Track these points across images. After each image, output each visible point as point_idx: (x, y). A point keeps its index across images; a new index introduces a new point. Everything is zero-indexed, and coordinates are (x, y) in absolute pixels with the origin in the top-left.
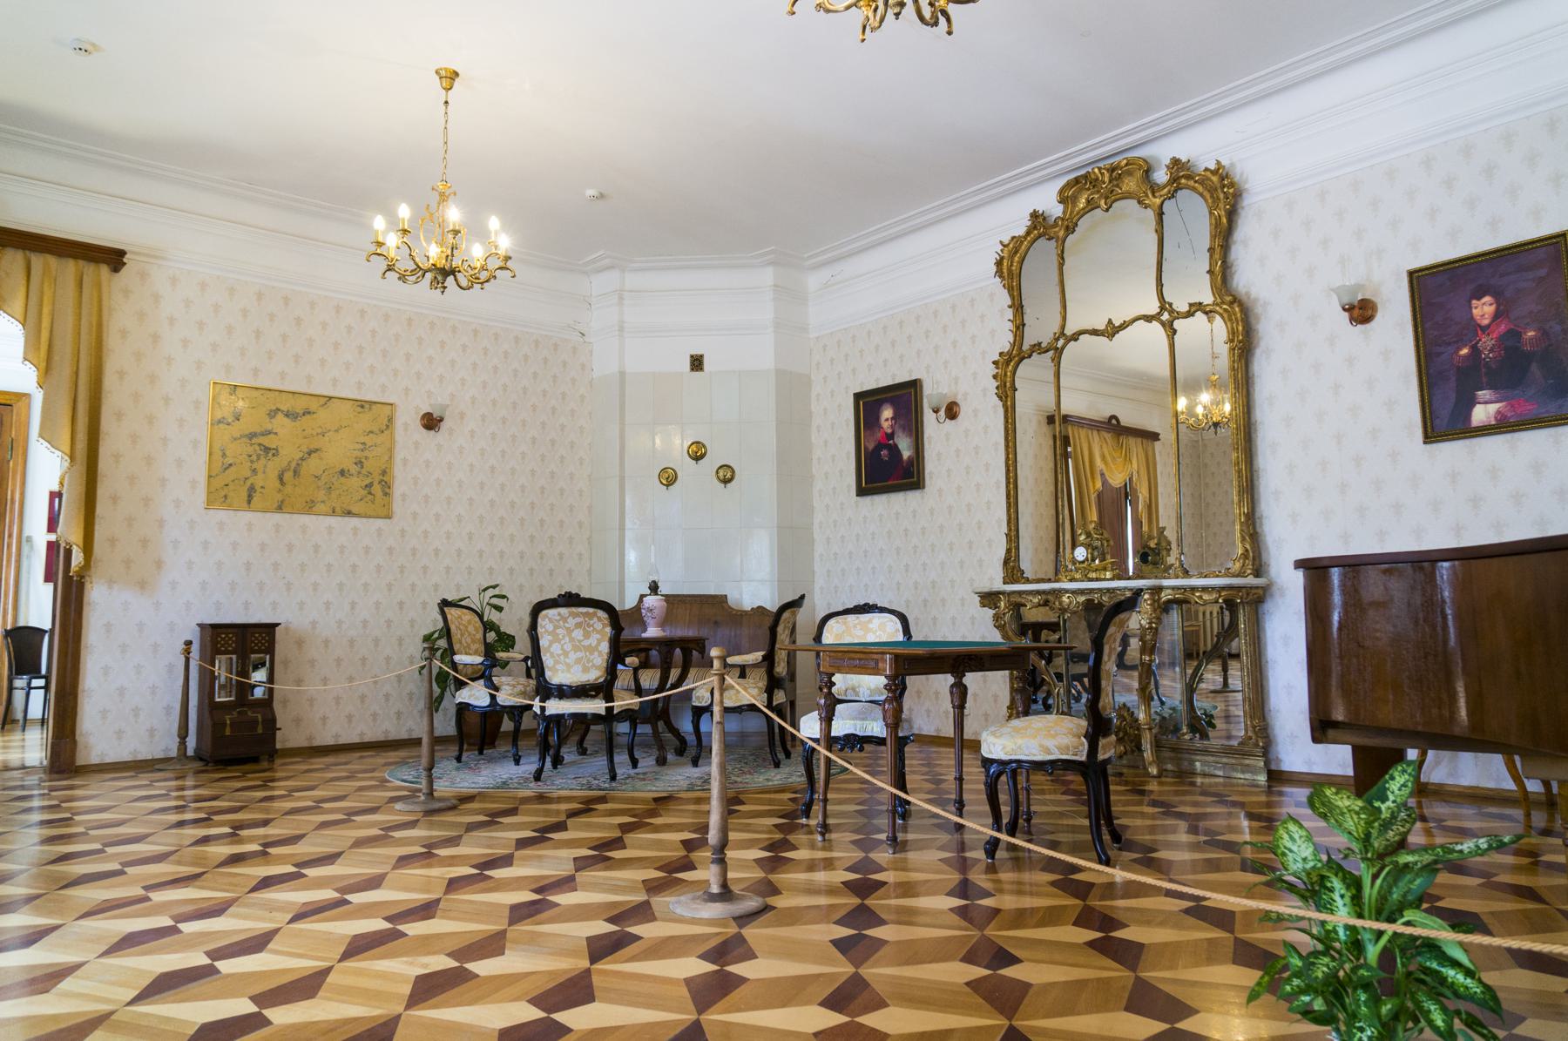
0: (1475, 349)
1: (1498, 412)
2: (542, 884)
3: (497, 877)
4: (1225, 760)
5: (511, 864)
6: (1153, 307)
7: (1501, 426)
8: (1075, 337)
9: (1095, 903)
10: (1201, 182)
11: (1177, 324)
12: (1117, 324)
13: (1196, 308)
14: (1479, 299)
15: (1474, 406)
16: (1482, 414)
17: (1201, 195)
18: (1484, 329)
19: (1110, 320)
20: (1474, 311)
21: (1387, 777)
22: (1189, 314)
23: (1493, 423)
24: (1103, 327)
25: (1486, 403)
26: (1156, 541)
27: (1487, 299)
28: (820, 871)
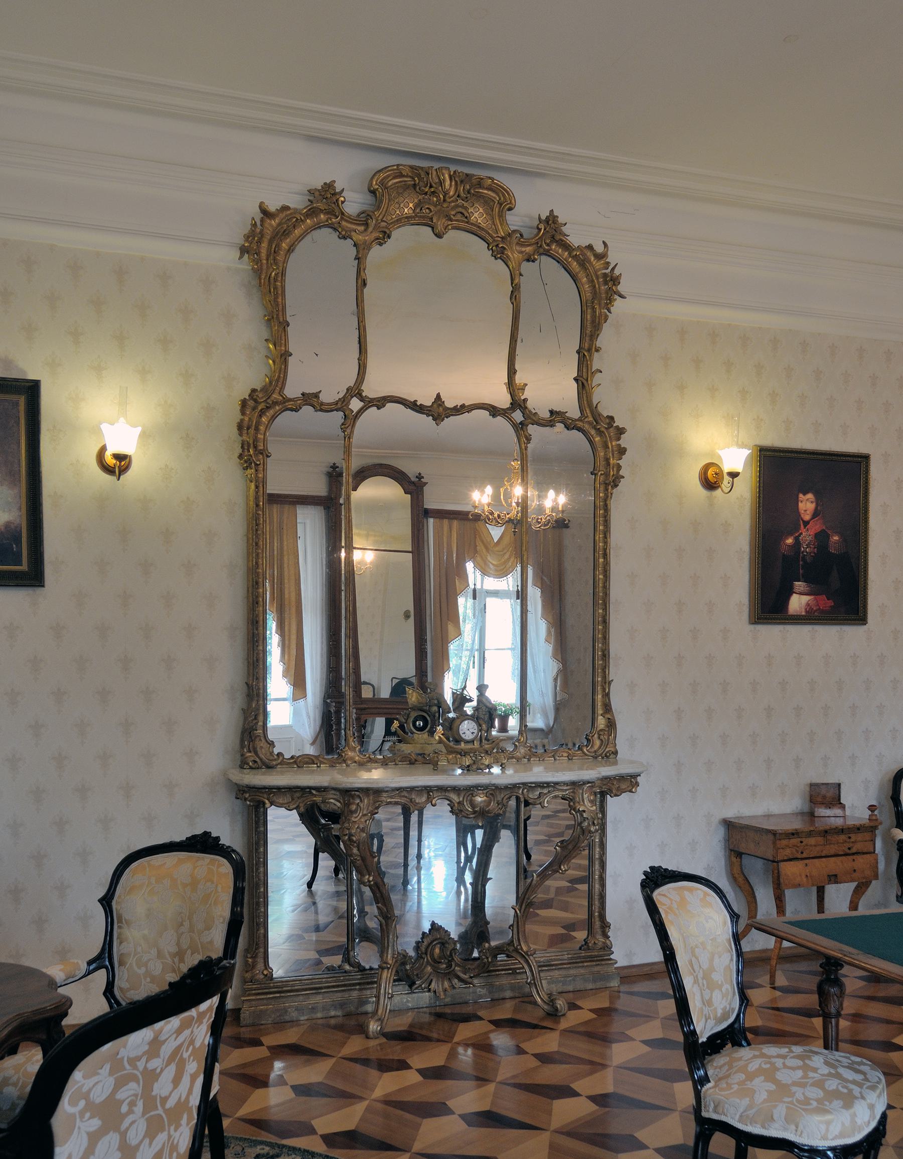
0: (797, 539)
1: (808, 604)
2: (806, 1019)
3: (542, 915)
4: (572, 972)
5: (543, 816)
6: (503, 399)
7: (809, 618)
8: (381, 402)
9: (833, 1071)
10: (583, 263)
11: (532, 429)
12: (449, 404)
13: (556, 417)
14: (804, 494)
15: (792, 595)
16: (797, 603)
17: (574, 278)
18: (806, 523)
19: (438, 396)
20: (800, 504)
21: (225, 1140)
22: (550, 424)
23: (804, 613)
24: (428, 403)
25: (801, 594)
26: (474, 703)
27: (810, 496)
28: (413, 1145)
